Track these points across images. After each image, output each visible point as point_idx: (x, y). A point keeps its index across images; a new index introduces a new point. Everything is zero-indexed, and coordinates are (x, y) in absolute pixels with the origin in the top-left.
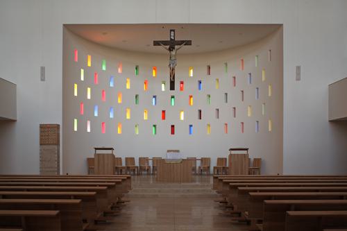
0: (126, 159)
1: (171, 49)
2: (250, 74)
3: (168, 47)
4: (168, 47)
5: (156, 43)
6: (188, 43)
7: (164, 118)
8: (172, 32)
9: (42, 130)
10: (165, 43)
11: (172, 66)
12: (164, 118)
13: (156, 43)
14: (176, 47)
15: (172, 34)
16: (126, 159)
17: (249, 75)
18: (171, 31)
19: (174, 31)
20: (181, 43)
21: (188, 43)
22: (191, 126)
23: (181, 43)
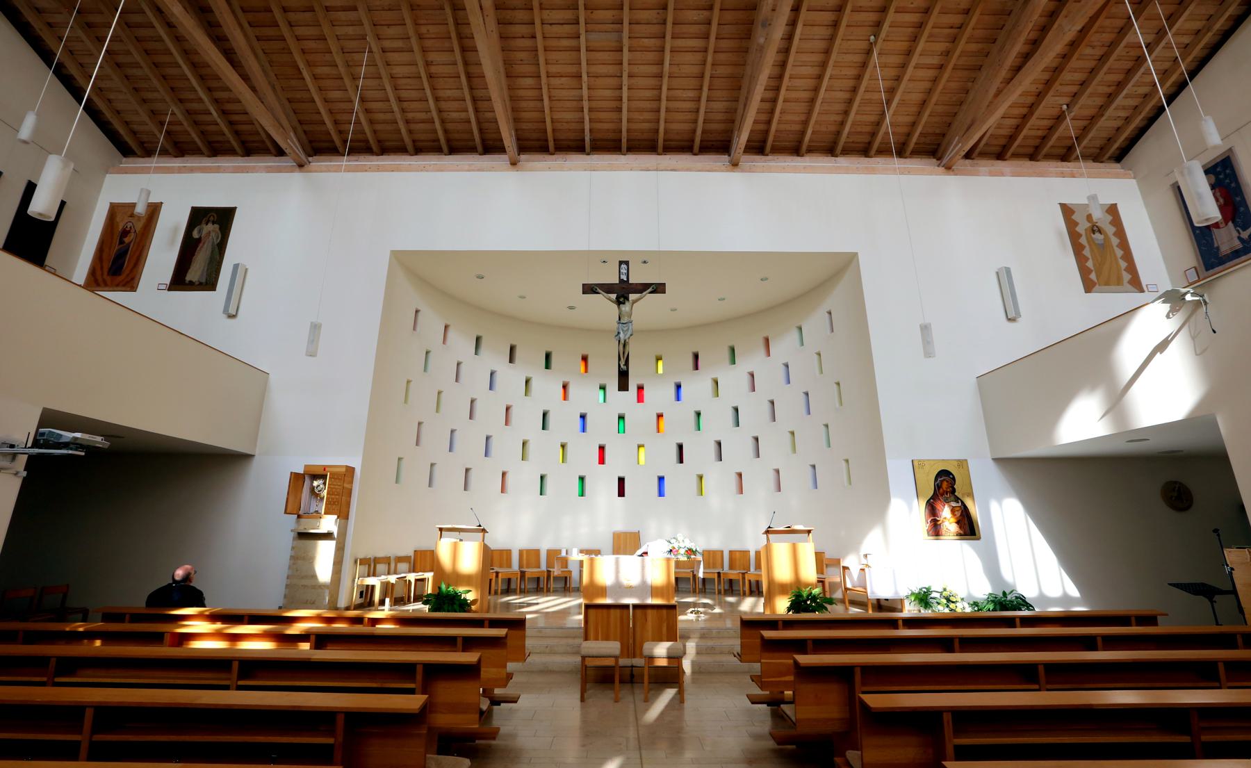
0: (521, 552)
1: (621, 300)
2: (847, 461)
3: (614, 296)
4: (614, 296)
5: (589, 289)
6: (659, 288)
7: (602, 460)
8: (624, 266)
9: (446, 22)
10: (608, 288)
11: (622, 335)
12: (602, 460)
13: (589, 289)
14: (632, 297)
15: (624, 271)
16: (521, 552)
17: (844, 464)
18: (621, 263)
19: (627, 263)
20: (642, 288)
21: (659, 288)
22: (660, 416)
23: (642, 288)
